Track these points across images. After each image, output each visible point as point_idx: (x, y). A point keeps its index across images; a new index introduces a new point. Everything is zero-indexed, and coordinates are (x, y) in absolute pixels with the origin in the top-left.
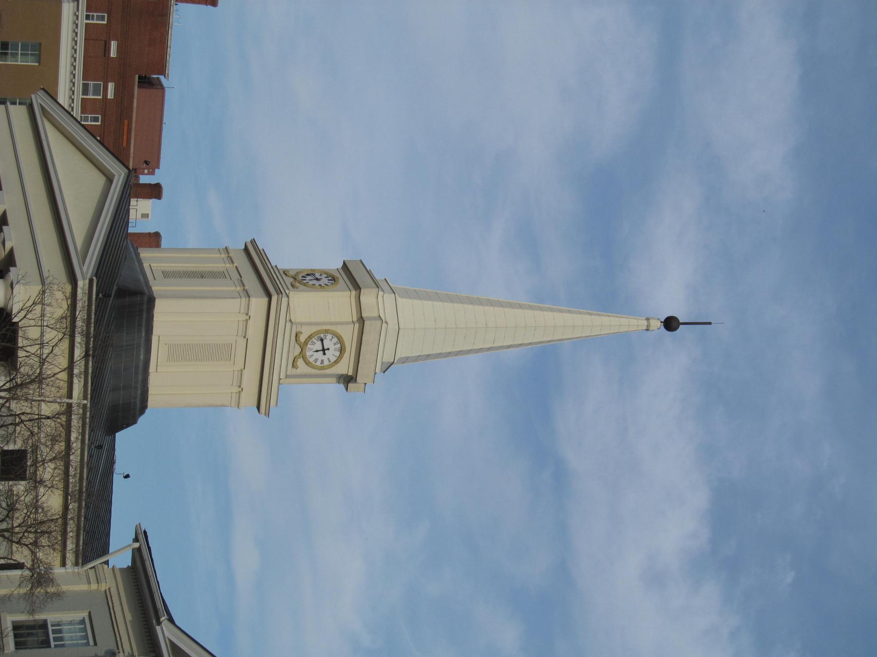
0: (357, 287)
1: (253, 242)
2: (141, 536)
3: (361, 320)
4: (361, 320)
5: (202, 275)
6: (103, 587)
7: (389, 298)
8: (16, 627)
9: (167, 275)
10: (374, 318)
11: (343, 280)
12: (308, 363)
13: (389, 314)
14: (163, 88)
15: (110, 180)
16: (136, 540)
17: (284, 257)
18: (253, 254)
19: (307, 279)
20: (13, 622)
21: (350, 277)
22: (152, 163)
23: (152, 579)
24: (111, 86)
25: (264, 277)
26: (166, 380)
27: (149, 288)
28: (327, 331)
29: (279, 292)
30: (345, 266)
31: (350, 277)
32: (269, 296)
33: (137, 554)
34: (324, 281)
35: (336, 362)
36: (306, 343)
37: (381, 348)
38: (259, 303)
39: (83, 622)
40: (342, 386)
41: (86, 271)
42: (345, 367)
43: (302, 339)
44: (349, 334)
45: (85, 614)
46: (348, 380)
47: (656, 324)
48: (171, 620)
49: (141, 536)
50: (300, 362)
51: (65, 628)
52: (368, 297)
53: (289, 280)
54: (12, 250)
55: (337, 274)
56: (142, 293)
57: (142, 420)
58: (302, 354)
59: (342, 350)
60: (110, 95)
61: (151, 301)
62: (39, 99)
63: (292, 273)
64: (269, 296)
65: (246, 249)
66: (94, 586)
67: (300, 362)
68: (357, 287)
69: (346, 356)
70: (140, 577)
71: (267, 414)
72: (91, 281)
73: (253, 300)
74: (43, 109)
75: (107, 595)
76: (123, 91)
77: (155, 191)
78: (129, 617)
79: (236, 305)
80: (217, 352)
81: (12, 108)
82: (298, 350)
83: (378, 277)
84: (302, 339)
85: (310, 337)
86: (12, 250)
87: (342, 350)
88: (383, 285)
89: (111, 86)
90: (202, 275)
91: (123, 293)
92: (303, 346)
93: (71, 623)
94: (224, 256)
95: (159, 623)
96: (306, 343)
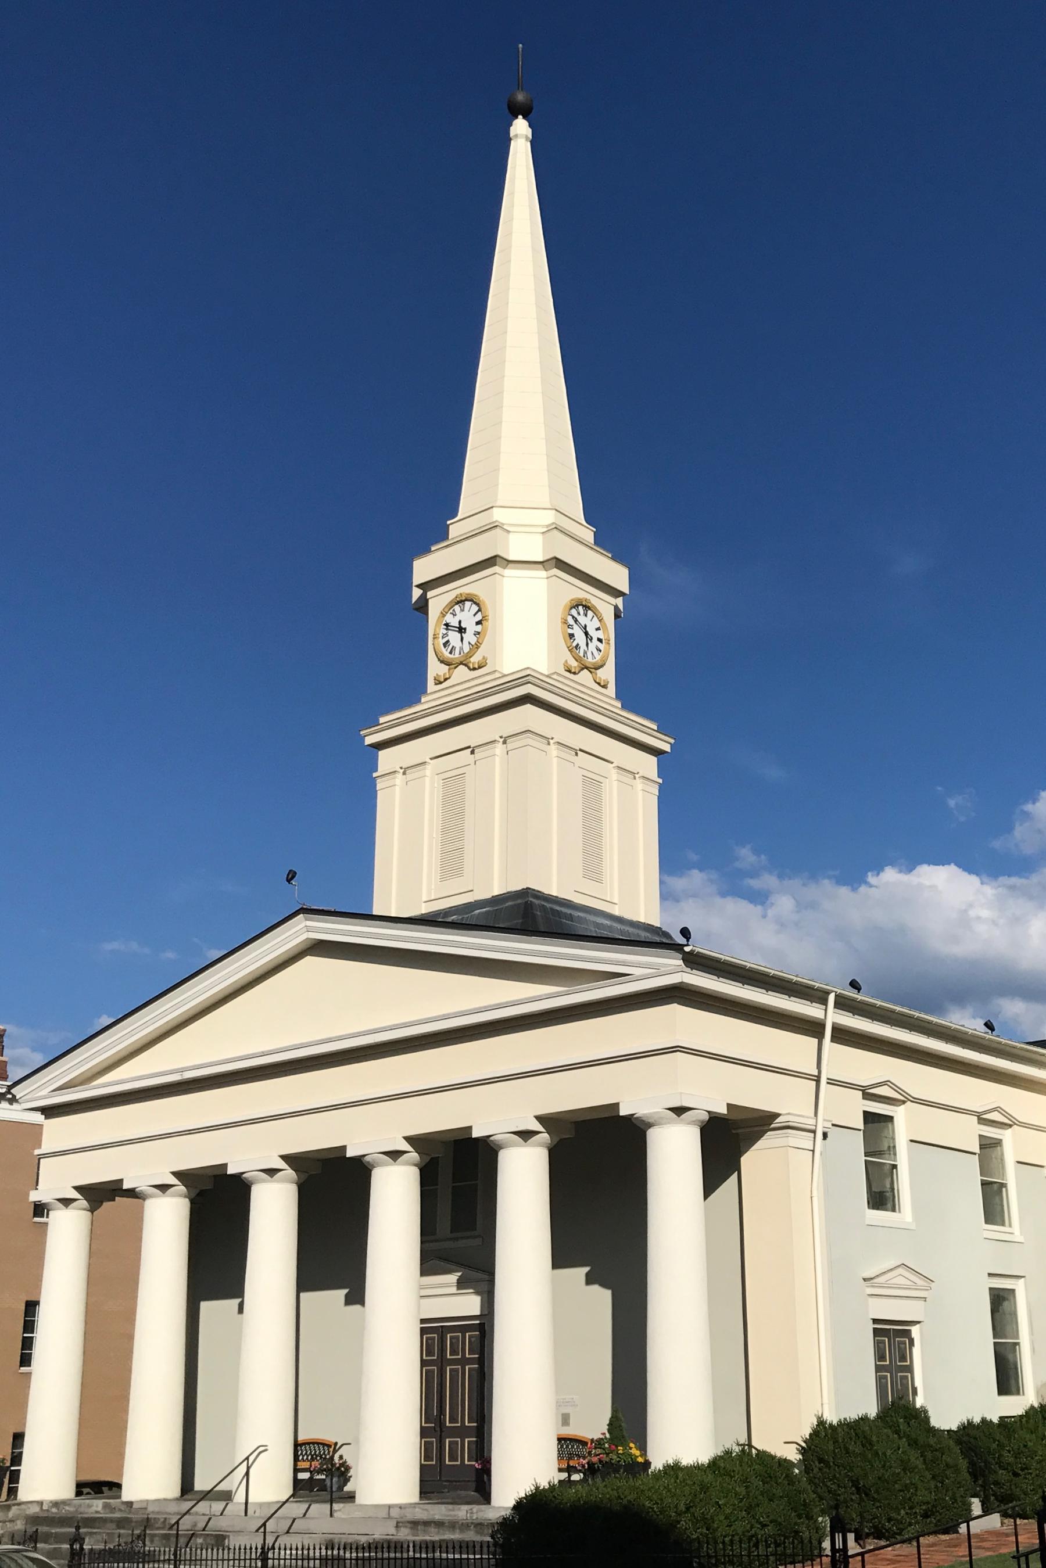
34: (467, 616)
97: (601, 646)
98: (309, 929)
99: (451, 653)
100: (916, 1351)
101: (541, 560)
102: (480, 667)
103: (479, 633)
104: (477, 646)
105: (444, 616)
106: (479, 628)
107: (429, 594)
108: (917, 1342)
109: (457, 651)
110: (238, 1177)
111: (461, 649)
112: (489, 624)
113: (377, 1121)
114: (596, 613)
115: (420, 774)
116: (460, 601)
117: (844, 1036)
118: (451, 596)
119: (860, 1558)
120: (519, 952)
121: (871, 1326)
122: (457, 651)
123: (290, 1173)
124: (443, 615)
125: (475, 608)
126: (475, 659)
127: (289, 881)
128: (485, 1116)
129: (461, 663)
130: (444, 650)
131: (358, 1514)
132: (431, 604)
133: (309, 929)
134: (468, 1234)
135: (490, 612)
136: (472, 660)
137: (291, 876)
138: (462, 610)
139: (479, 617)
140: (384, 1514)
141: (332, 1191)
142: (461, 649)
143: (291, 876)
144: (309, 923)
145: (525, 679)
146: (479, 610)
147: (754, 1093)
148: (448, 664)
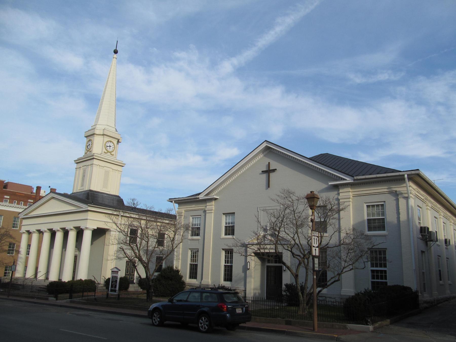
0: (94, 134)
1: (75, 161)
2: (171, 200)
3: (103, 135)
4: (103, 135)
5: (84, 176)
6: (183, 212)
7: (98, 126)
8: (192, 235)
9: (82, 185)
10: (103, 132)
11: (91, 138)
12: (113, 151)
13: (103, 127)
14: (8, 183)
15: (53, 198)
16: (172, 202)
17: (81, 153)
18: (78, 162)
19: (89, 148)
20: (226, 234)
21: (90, 136)
22: (31, 188)
23: (183, 199)
24: (6, 197)
25: (87, 159)
26: (112, 190)
27: (86, 191)
28: (105, 145)
29: (93, 156)
30: (86, 137)
31: (90, 136)
32: (94, 158)
33: (176, 202)
34: (90, 143)
35: (114, 144)
36: (107, 151)
37: (111, 131)
38: (95, 162)
39: (193, 218)
40: (119, 143)
41: (84, 207)
42: (115, 142)
43: (106, 152)
44: (107, 139)
45: (191, 218)
46: (118, 142)
47: (115, 56)
48: (199, 194)
49: (171, 200)
50: (112, 153)
51: (228, 221)
52: (97, 132)
53: (88, 153)
54: (61, 228)
55: (88, 139)
56: (88, 193)
57: (122, 198)
58: (110, 152)
59: (111, 142)
60: (8, 197)
61: (91, 191)
62: (21, 216)
63: (86, 152)
64: (94, 158)
65: (77, 163)
66: (213, 211)
67: (112, 153)
68: (94, 134)
69: (112, 141)
70: (181, 202)
71: (125, 164)
72: (89, 206)
73: (94, 163)
74: (344, 179)
75: (186, 211)
76: (7, 193)
77: (39, 188)
78: (194, 206)
79: (95, 168)
80: (107, 174)
81: (23, 224)
82: (109, 153)
83: (90, 128)
84: (106, 152)
85: (106, 149)
86: (61, 228)
87: (111, 142)
88: (93, 127)
89: (6, 197)
90: (84, 176)
91: (88, 198)
92: (108, 152)
93: (226, 219)
94: (78, 169)
95: (199, 198)
96: (107, 151)
123: (48, 231)
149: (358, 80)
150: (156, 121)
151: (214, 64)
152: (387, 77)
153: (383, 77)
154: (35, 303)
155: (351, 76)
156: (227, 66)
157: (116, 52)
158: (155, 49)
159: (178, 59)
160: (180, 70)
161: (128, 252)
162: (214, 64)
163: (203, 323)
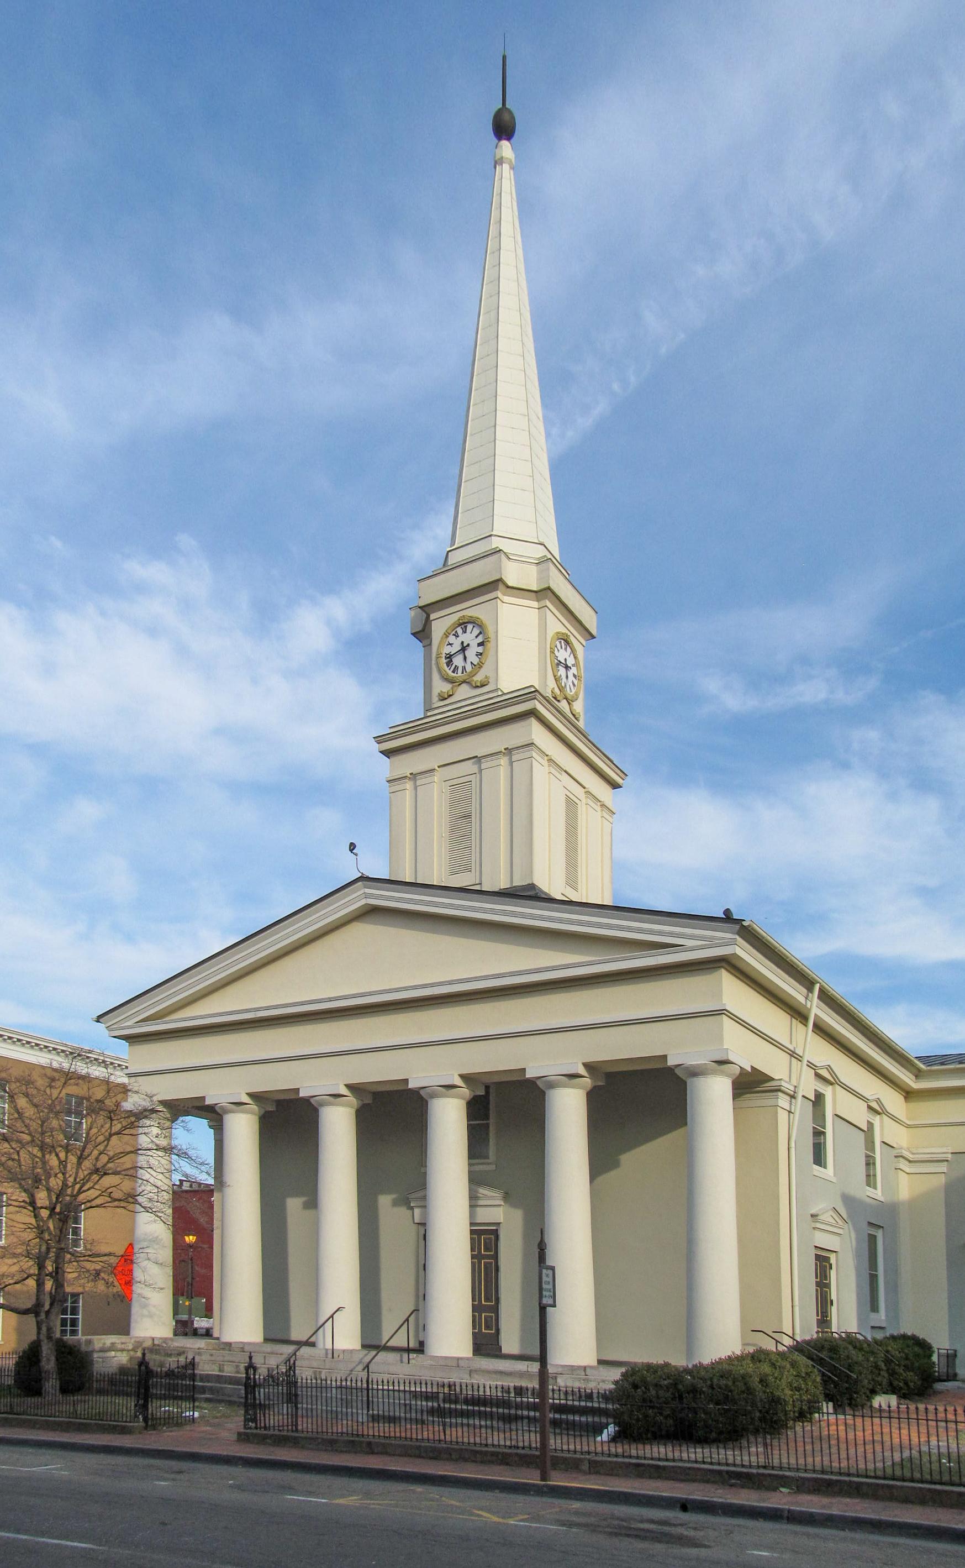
0: (495, 584)
1: (379, 739)
34: (470, 637)
47: (506, 149)
65: (388, 753)
68: (495, 584)
97: (576, 682)
98: (367, 896)
99: (453, 672)
100: (833, 1273)
101: (535, 589)
102: (482, 686)
103: (481, 654)
104: (480, 666)
105: (447, 637)
106: (480, 649)
107: (432, 617)
108: (834, 1266)
109: (460, 670)
110: (307, 1101)
111: (464, 668)
112: (490, 646)
113: (438, 1060)
114: (573, 652)
115: (429, 780)
116: (463, 624)
117: (821, 1030)
118: (455, 618)
119: (537, 1352)
120: (600, 926)
121: (814, 1252)
122: (460, 670)
123: (352, 1099)
124: (446, 635)
125: (476, 631)
126: (478, 678)
127: (351, 850)
128: (419, 1072)
129: (464, 682)
130: (447, 669)
131: (430, 1362)
132: (435, 625)
133: (367, 896)
134: (483, 1161)
135: (491, 633)
136: (475, 678)
137: (352, 847)
138: (465, 632)
139: (480, 639)
140: (454, 1364)
141: (392, 1117)
142: (464, 668)
143: (352, 847)
144: (367, 891)
145: (532, 693)
146: (480, 633)
147: (774, 1065)
148: (451, 681)
149: (732, 699)
150: (87, 811)
151: (266, 617)
152: (822, 696)
153: (812, 691)
154: (773, 1515)
155: (712, 685)
156: (313, 626)
157: (503, 128)
158: (57, 543)
159: (142, 589)
160: (153, 631)
161: (813, 1208)
162: (266, 617)
163: (585, 1467)
